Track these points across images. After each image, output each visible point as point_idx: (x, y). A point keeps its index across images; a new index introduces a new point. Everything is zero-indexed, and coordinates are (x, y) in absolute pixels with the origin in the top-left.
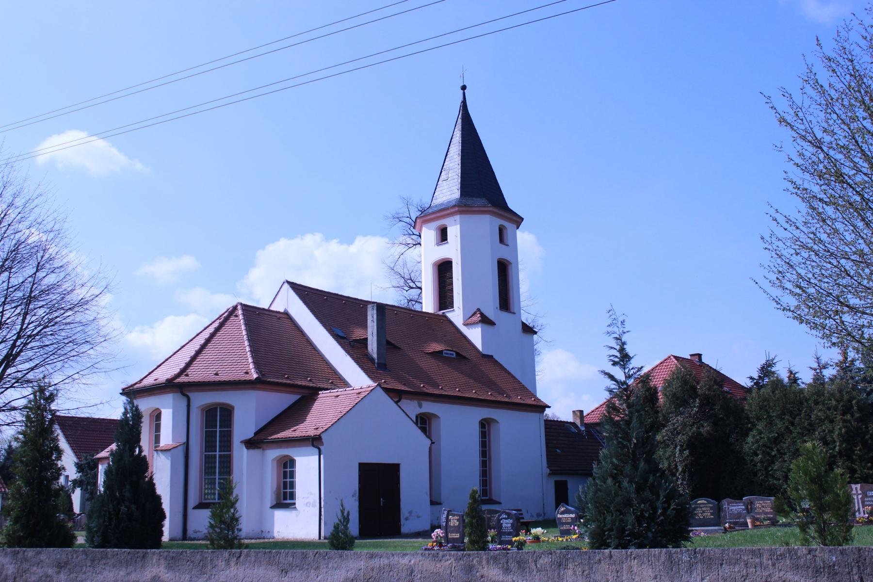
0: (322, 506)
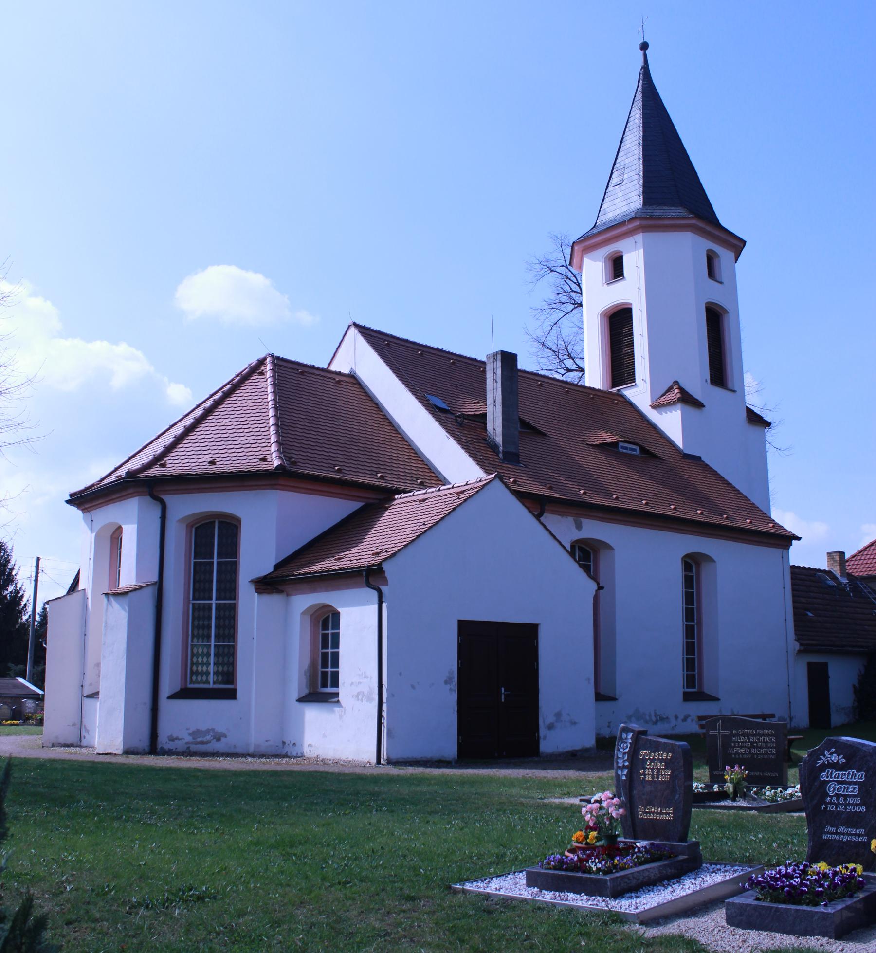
0: (384, 700)
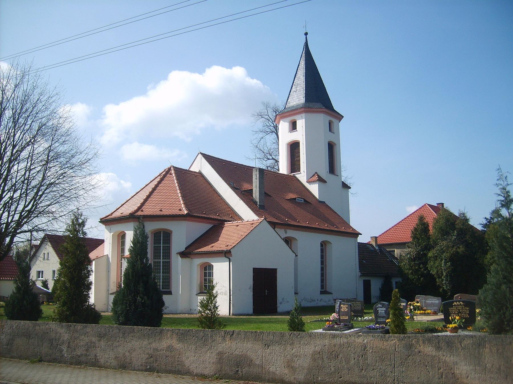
0: (231, 295)
